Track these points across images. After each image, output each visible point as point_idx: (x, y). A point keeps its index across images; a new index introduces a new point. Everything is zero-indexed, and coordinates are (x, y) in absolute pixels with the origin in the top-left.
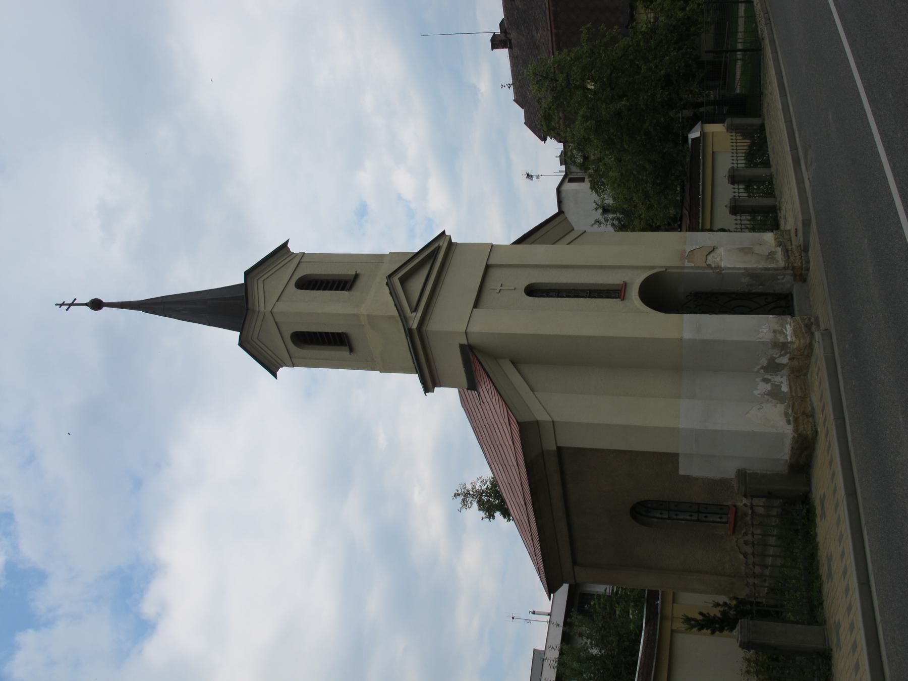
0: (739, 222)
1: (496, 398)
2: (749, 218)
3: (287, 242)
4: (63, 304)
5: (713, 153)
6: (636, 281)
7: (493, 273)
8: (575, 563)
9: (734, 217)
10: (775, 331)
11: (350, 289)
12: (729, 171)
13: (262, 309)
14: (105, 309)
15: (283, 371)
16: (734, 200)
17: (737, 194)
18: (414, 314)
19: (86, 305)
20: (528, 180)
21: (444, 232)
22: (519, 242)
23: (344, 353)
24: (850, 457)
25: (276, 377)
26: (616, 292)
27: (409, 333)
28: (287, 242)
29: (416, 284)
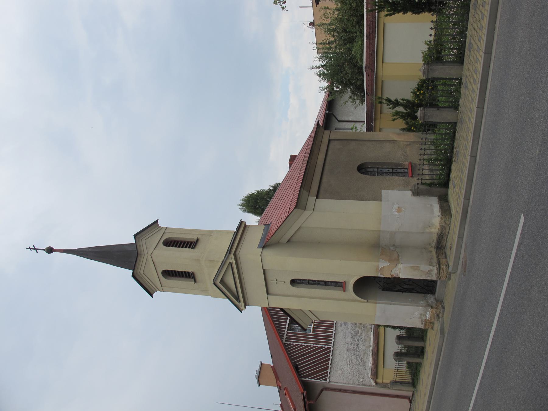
3: (157, 221)
10: (421, 314)
11: (194, 248)
13: (146, 253)
15: (156, 294)
19: (44, 250)
23: (188, 283)
26: (341, 285)
28: (157, 221)
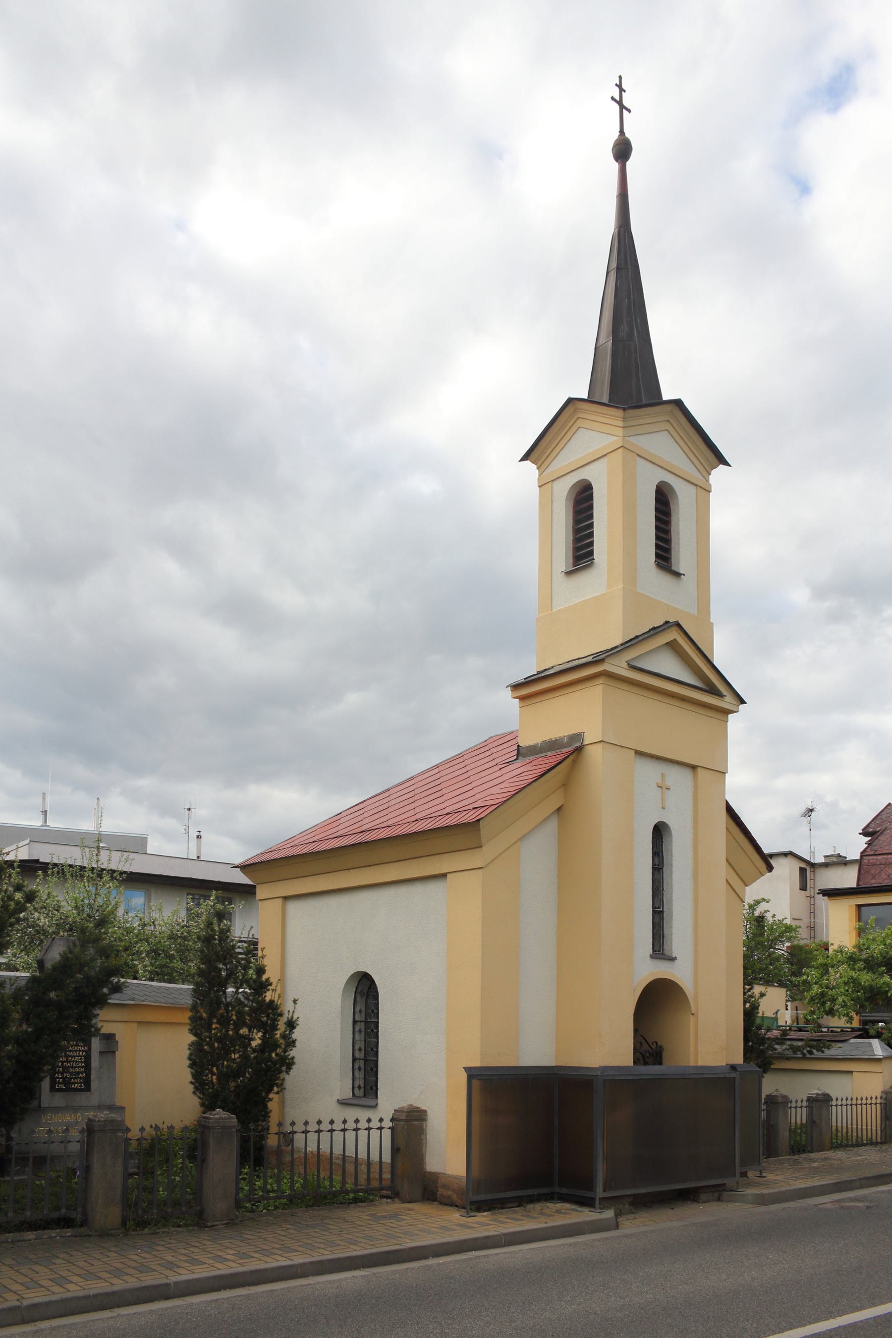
0: (799, 1104)
1: (510, 787)
2: (804, 1121)
3: (726, 463)
4: (622, 90)
5: (851, 1072)
6: (681, 972)
7: (687, 774)
8: (286, 898)
9: (805, 1099)
12: (785, 1097)
14: (616, 166)
16: (786, 1101)
17: (794, 1105)
18: (625, 665)
19: (622, 132)
20: (803, 810)
21: (743, 702)
22: (730, 810)
24: (225, 1288)
25: (521, 461)
26: (660, 948)
27: (598, 659)
28: (726, 463)
29: (669, 665)
